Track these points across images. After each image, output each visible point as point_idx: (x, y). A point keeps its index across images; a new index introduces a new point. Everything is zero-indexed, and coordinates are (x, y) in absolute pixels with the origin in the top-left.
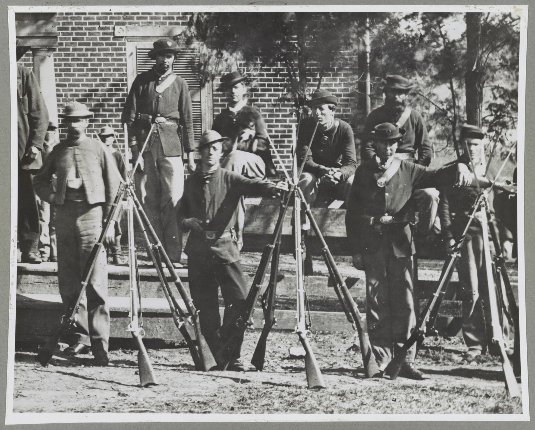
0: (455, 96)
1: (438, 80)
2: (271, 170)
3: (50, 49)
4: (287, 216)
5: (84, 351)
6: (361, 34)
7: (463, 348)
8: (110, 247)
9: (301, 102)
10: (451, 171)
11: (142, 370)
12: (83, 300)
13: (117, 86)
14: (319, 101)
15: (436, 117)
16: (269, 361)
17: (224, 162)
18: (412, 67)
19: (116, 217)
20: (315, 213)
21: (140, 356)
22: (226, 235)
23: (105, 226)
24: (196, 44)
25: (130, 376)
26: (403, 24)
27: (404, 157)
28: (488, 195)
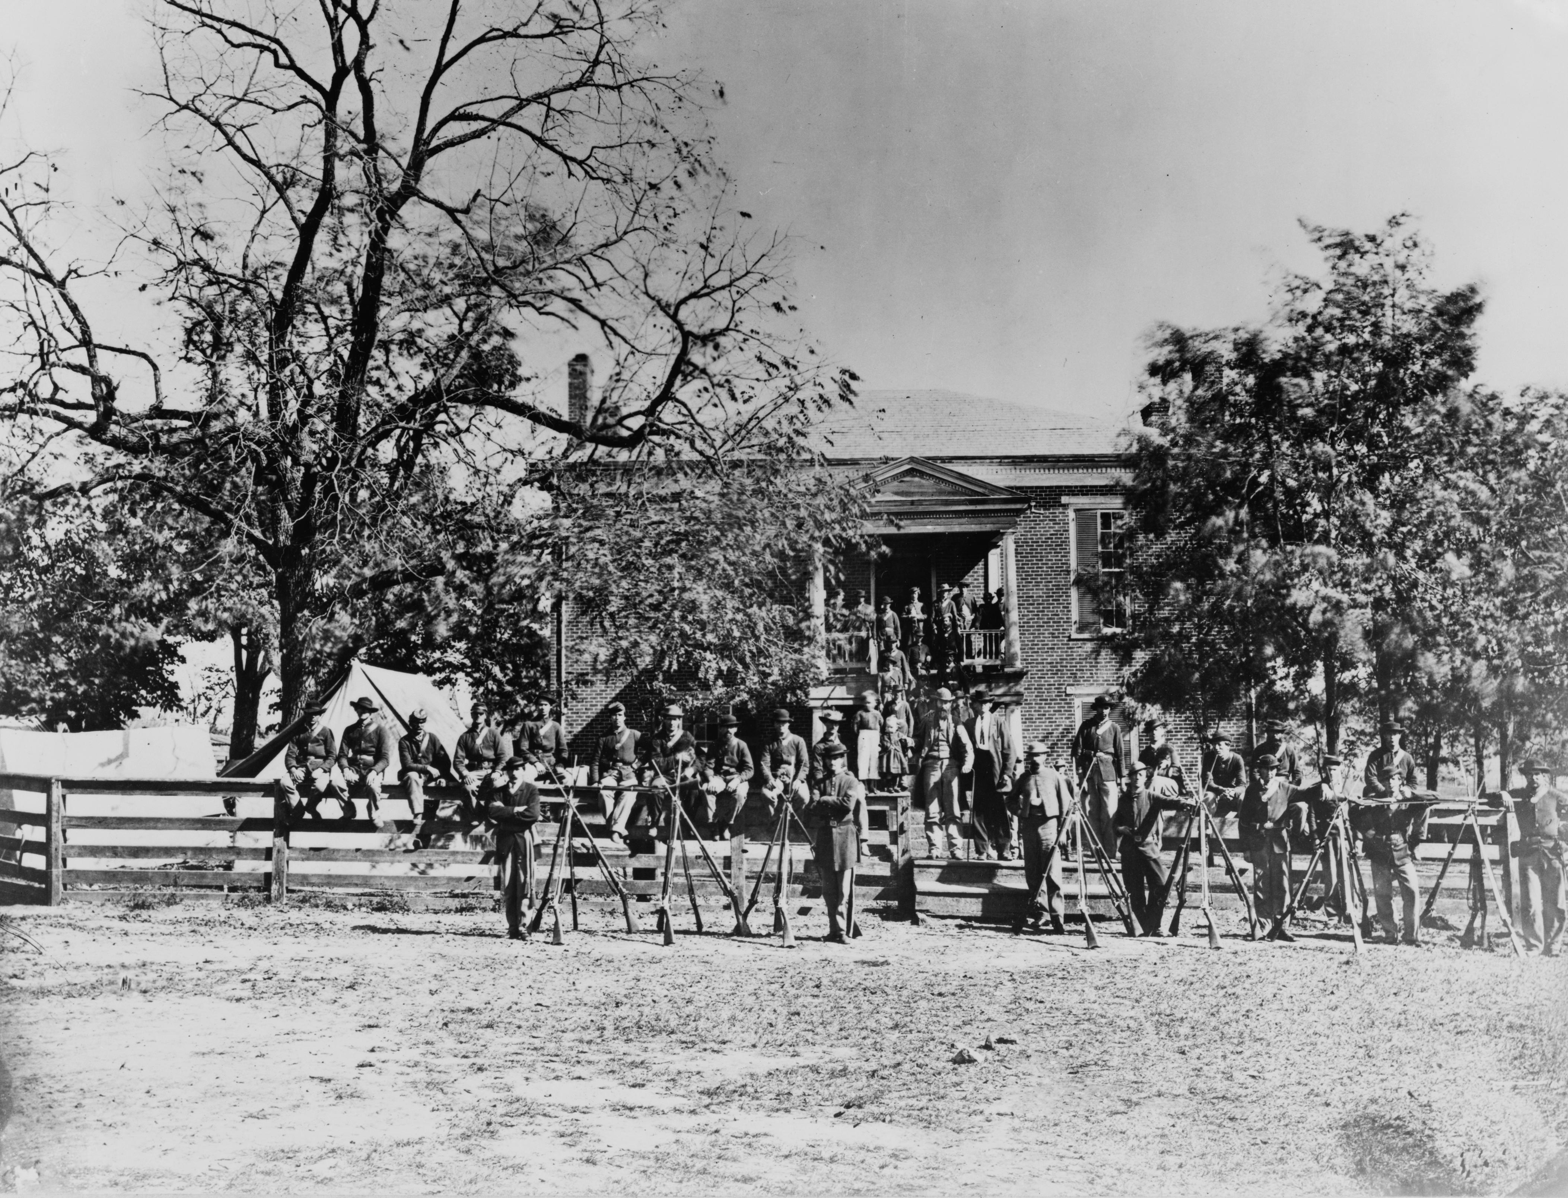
0: (1319, 734)
1: (1305, 723)
2: (1182, 789)
3: (1018, 703)
4: (1195, 824)
5: (1046, 923)
6: (1248, 690)
7: (1325, 918)
8: (1063, 848)
9: (1204, 740)
10: (1316, 790)
11: (1090, 938)
12: (1044, 886)
13: (1068, 730)
14: (1217, 739)
15: (1304, 749)
16: (1181, 929)
17: (1147, 784)
18: (1287, 714)
19: (1068, 826)
20: (1216, 821)
21: (1088, 927)
22: (1149, 839)
23: (1059, 833)
24: (1126, 699)
25: (1080, 941)
26: (1279, 683)
27: (1282, 779)
28: (1344, 807)
